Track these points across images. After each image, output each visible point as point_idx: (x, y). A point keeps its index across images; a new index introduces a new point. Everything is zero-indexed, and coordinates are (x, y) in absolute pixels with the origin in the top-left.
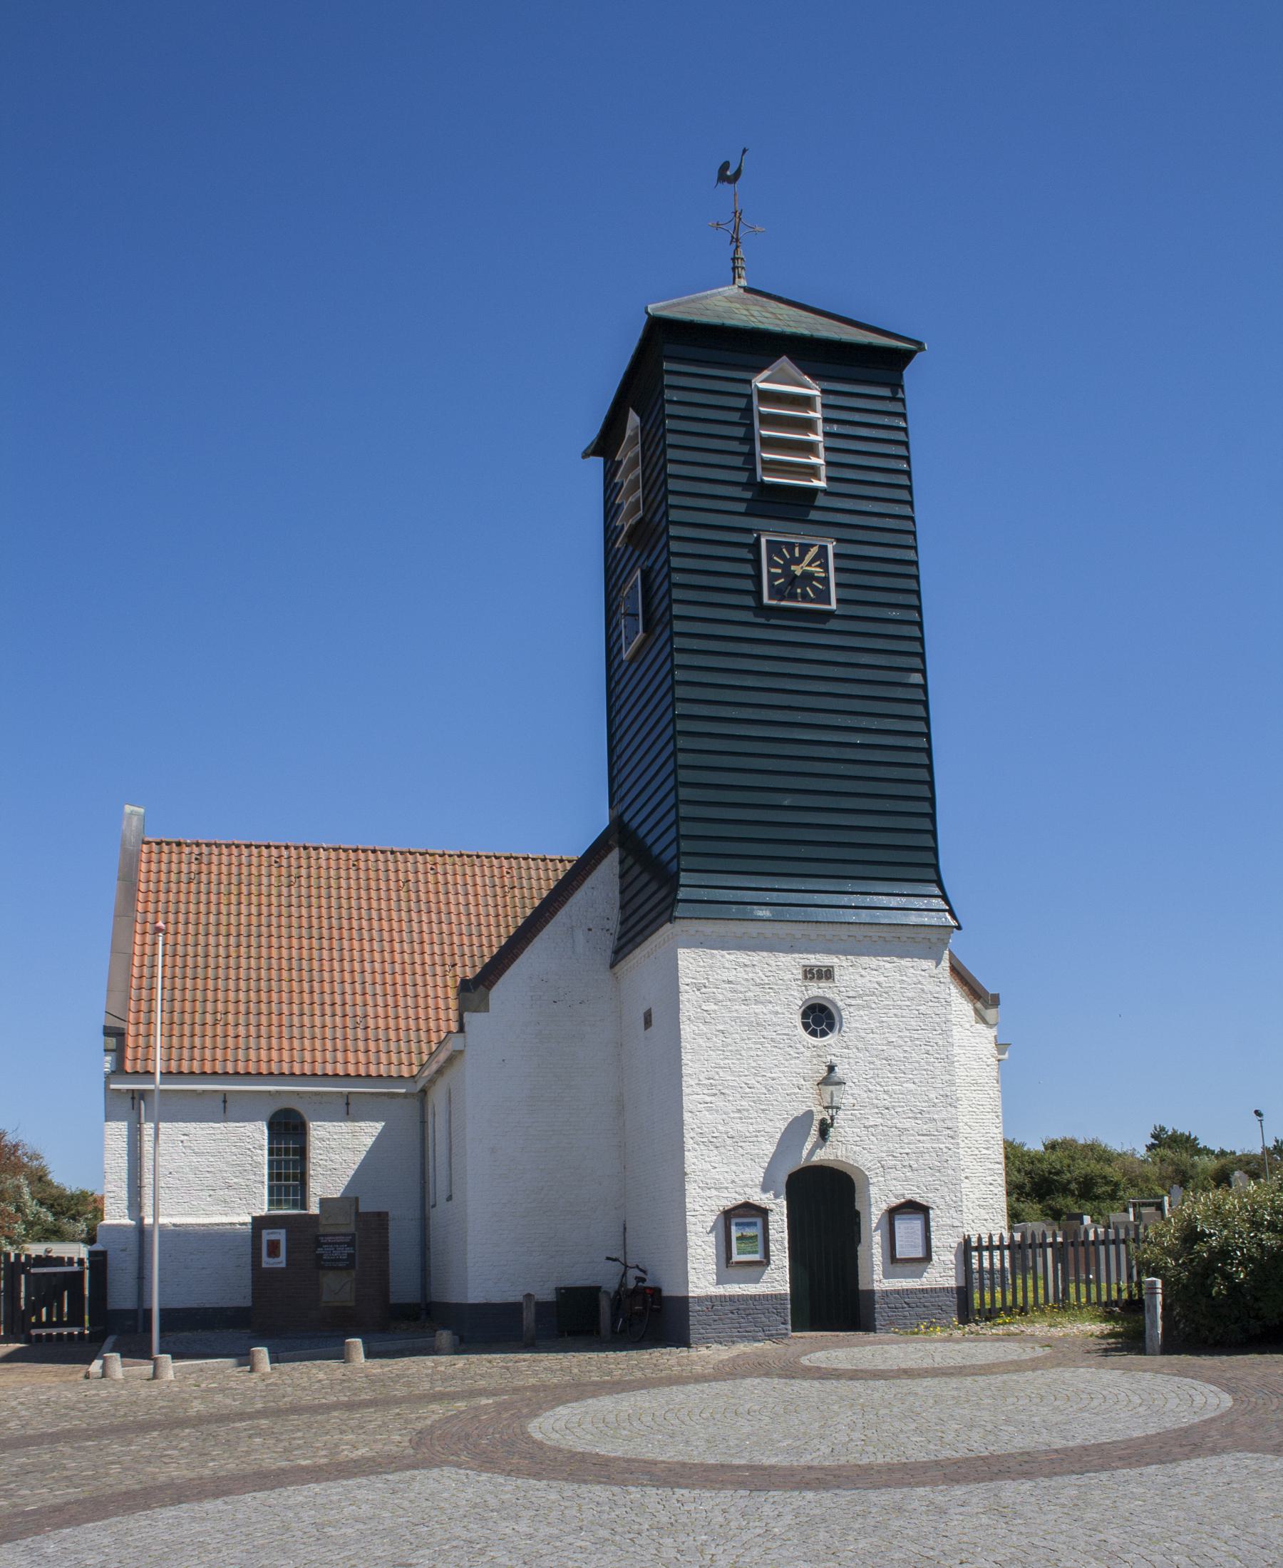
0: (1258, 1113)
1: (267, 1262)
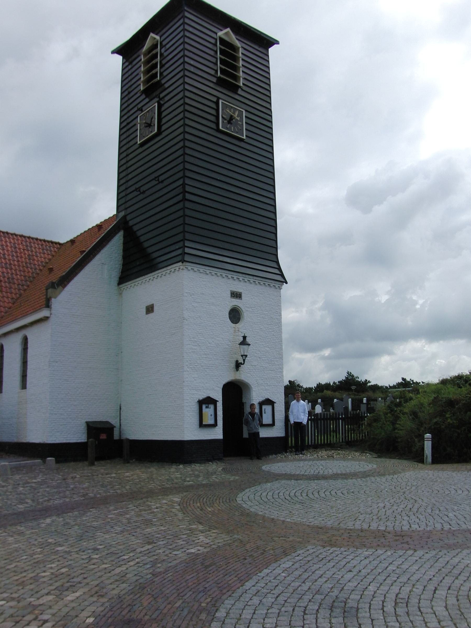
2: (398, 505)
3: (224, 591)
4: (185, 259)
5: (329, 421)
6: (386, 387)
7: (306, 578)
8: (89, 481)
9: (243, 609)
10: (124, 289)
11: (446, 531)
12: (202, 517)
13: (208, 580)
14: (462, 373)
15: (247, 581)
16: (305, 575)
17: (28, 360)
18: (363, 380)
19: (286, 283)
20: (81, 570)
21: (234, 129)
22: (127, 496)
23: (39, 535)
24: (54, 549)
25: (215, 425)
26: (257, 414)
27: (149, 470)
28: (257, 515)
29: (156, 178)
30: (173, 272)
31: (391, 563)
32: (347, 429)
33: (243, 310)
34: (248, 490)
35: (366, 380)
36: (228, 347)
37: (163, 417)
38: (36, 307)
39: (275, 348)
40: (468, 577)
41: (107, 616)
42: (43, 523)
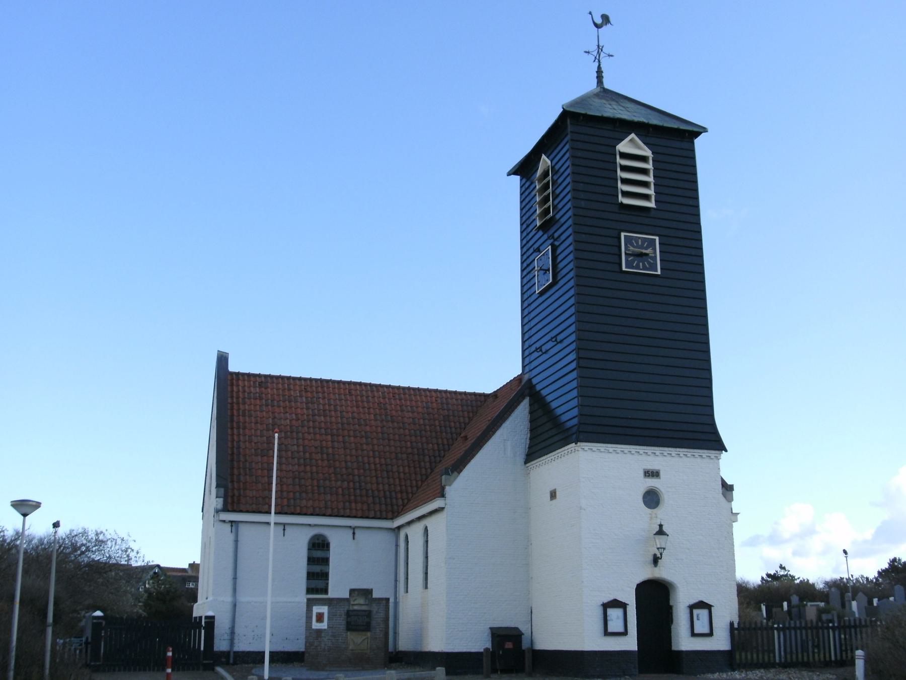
0: (845, 552)
1: (316, 625)
21: (644, 265)
29: (552, 338)
30: (571, 453)
33: (663, 490)
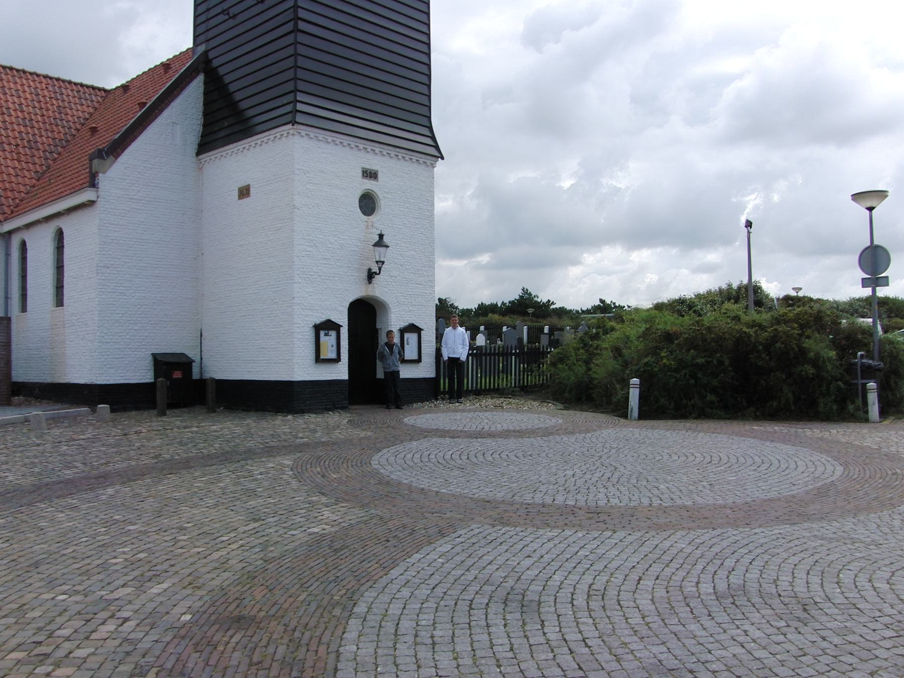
2: (592, 473)
3: (363, 581)
4: (297, 120)
5: (497, 357)
6: (577, 312)
7: (471, 564)
8: (161, 437)
9: (390, 603)
10: (205, 161)
11: (655, 507)
12: (325, 486)
13: (339, 568)
14: (684, 295)
15: (392, 569)
16: (469, 562)
17: (65, 264)
18: (545, 300)
19: (443, 158)
20: (166, 554)
22: (218, 457)
23: (101, 510)
24: (123, 528)
25: (338, 360)
26: (397, 345)
27: (245, 422)
28: (400, 483)
30: (254, 147)
31: (583, 547)
32: (522, 369)
33: (380, 196)
34: (387, 449)
35: (549, 301)
36: (357, 249)
37: (264, 348)
38: (74, 185)
39: (424, 252)
40: (682, 565)
41: (208, 612)
42: (103, 494)
